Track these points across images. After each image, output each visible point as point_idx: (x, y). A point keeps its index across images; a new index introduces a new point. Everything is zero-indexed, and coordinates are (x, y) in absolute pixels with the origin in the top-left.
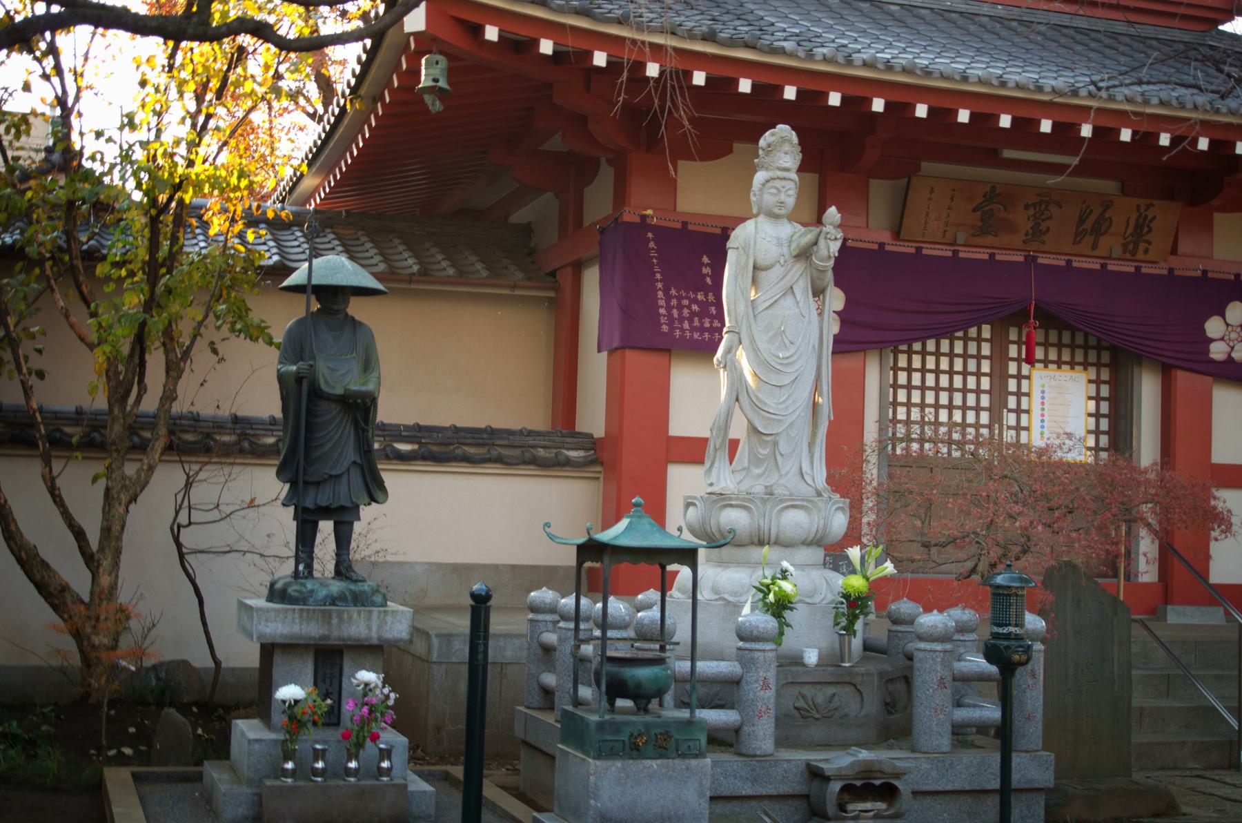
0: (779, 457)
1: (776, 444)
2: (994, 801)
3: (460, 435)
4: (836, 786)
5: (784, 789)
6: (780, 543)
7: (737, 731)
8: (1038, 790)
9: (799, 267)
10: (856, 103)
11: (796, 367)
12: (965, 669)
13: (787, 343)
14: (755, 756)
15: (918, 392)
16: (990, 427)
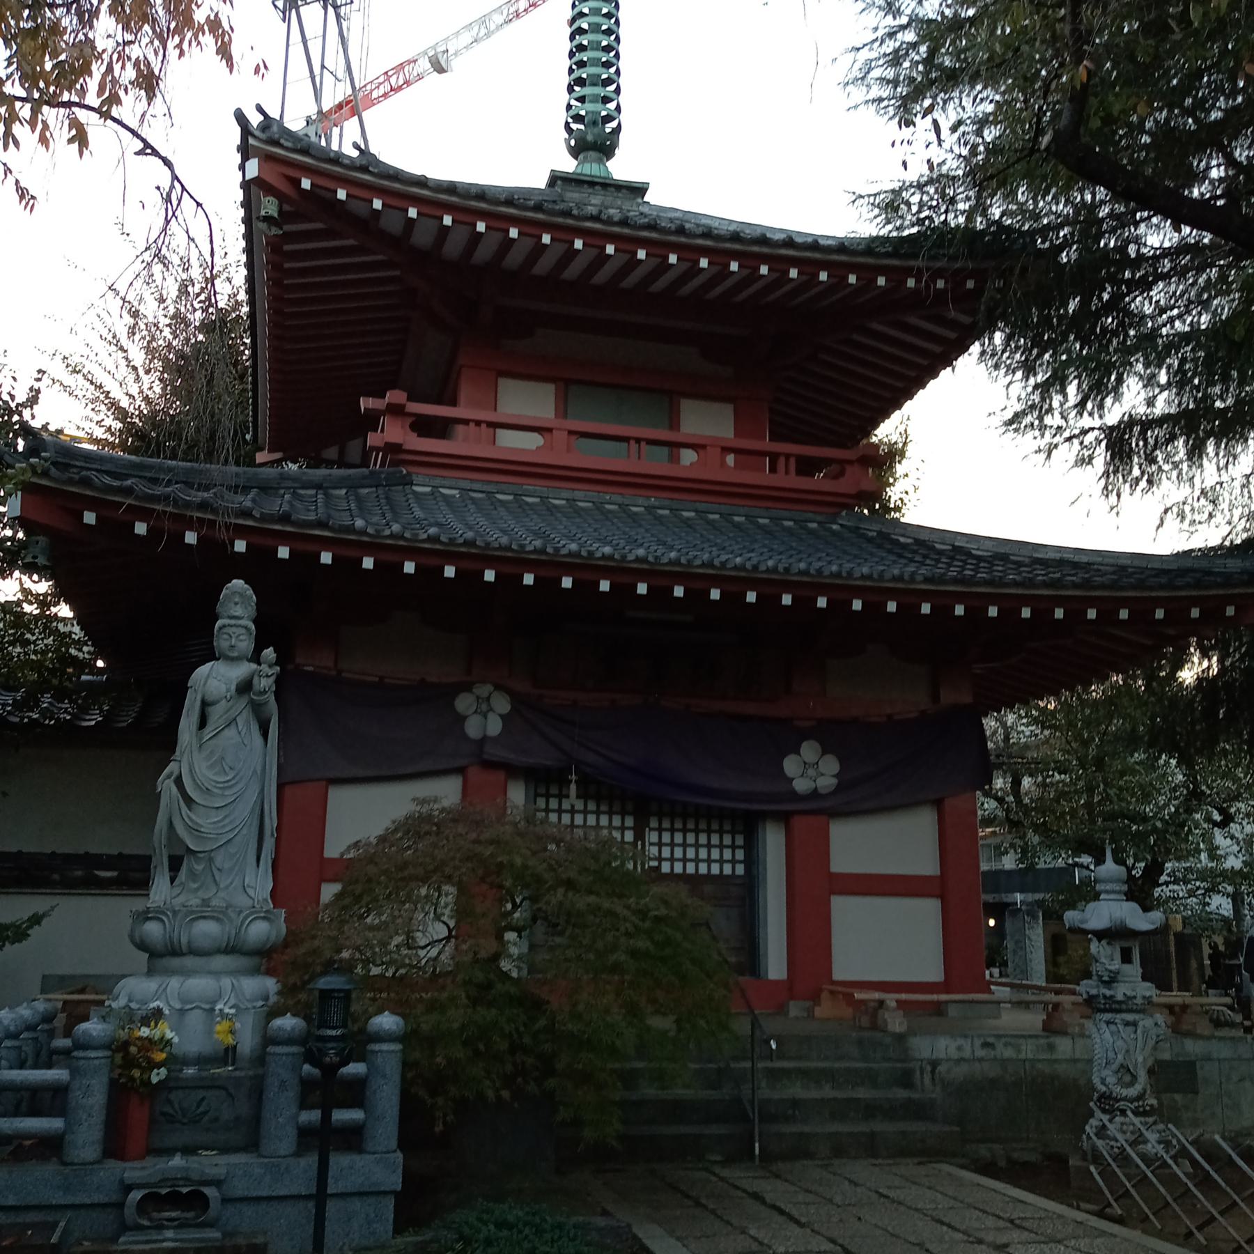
0: (216, 872)
1: (211, 860)
6: (194, 952)
8: (385, 1193)
9: (243, 701)
10: (305, 558)
11: (235, 790)
12: (31, 1078)
13: (227, 769)
14: (72, 1164)
15: (569, 815)
16: (635, 844)
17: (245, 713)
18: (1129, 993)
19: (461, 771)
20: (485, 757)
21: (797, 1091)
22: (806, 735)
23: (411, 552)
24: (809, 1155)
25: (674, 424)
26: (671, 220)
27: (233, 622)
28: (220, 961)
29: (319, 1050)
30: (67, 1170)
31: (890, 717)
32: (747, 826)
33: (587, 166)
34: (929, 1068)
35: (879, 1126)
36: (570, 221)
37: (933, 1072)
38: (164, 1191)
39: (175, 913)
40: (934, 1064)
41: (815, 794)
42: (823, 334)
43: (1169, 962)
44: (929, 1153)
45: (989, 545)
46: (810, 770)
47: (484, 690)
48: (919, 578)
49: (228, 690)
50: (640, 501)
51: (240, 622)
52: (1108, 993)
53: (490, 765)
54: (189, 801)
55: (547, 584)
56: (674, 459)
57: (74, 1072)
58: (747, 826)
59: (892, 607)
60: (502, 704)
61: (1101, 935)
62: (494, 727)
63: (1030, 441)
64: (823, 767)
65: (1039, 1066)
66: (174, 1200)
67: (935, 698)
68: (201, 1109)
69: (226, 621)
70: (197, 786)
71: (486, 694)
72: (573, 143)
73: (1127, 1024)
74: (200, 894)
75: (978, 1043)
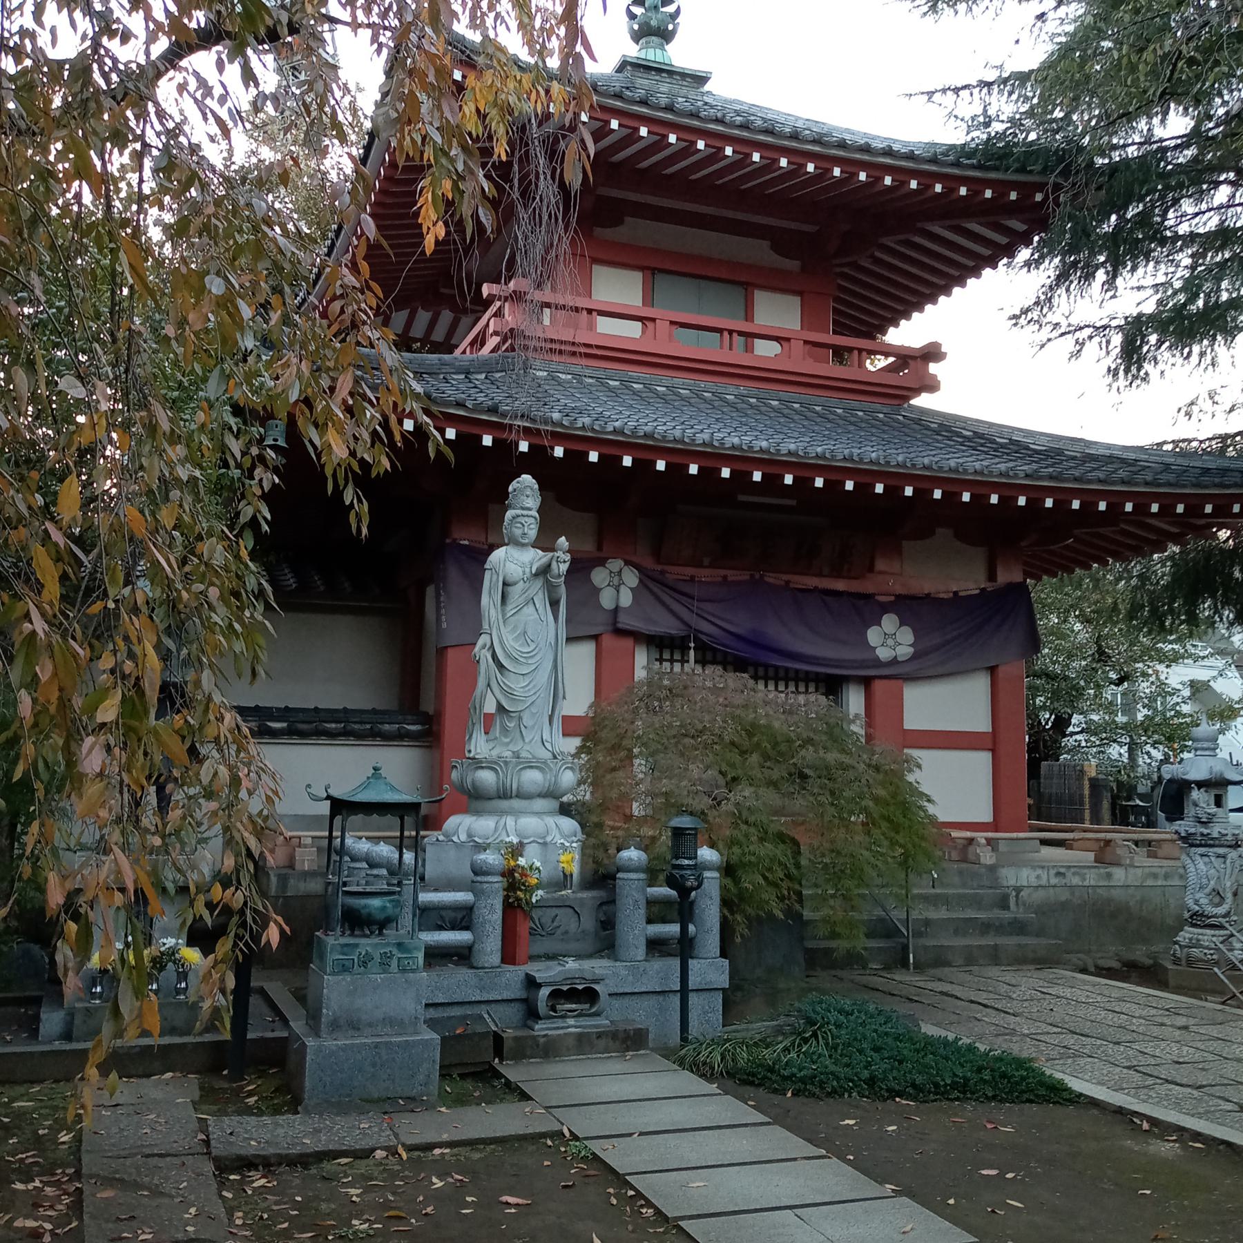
1: (520, 718)
2: (676, 1000)
3: (332, 715)
4: (544, 992)
5: (506, 995)
6: (521, 795)
7: (470, 948)
9: (539, 583)
10: (575, 457)
11: (537, 658)
17: (540, 593)
18: (1224, 832)
19: (596, 638)
20: (620, 626)
21: (933, 914)
22: (885, 609)
23: (596, 442)
24: (948, 964)
25: (749, 316)
26: (738, 113)
27: (525, 512)
28: (540, 804)
29: (682, 876)
30: (481, 972)
31: (956, 593)
32: (833, 686)
33: (651, 51)
34: (1014, 893)
35: (1002, 941)
36: (696, 123)
37: (1017, 896)
38: (565, 988)
39: (506, 763)
40: (1018, 890)
41: (894, 662)
42: (863, 231)
43: (1082, 804)
44: (1043, 962)
45: (1043, 441)
46: (890, 639)
47: (615, 564)
48: (1022, 474)
49: (524, 573)
50: (731, 389)
51: (530, 513)
52: (1206, 831)
53: (620, 632)
54: (500, 666)
55: (675, 469)
56: (749, 349)
57: (644, 892)
58: (833, 686)
59: (966, 497)
60: (631, 578)
61: (1200, 784)
62: (626, 599)
63: (1028, 334)
64: (899, 638)
65: (1099, 891)
66: (573, 995)
67: (992, 577)
68: (555, 924)
69: (519, 512)
70: (509, 656)
71: (616, 570)
72: (636, 27)
73: (1219, 856)
74: (511, 747)
75: (1052, 872)
